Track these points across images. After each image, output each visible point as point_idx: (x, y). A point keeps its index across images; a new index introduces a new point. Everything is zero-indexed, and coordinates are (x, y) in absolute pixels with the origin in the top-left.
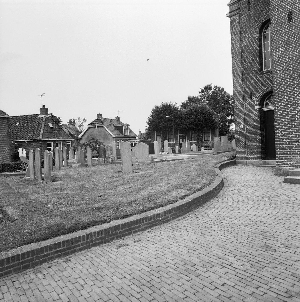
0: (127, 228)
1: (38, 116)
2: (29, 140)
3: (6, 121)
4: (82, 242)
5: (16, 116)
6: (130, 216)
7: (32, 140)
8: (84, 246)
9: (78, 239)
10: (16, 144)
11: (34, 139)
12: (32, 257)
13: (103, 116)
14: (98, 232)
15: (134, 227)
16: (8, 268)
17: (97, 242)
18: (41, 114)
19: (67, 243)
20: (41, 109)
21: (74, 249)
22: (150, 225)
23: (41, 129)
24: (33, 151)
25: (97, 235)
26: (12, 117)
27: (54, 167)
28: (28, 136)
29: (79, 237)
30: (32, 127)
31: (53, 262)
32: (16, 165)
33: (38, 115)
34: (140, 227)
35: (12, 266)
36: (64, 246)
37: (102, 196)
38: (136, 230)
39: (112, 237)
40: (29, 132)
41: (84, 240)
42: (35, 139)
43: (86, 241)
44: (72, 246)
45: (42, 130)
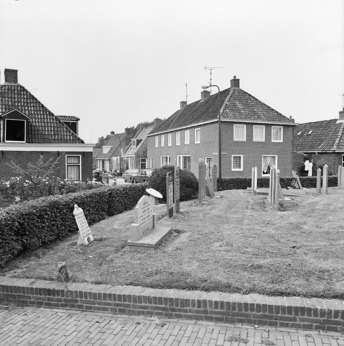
0: (267, 313)
1: (336, 122)
2: (320, 152)
3: (291, 129)
4: (190, 308)
5: (311, 123)
6: (286, 296)
7: (324, 151)
8: (193, 314)
9: (186, 302)
10: (305, 155)
11: (326, 151)
12: (128, 303)
13: (295, 122)
14: (216, 303)
15: (282, 317)
16: (105, 304)
17: (214, 316)
18: (341, 118)
19: (170, 301)
20: (340, 113)
21: (179, 313)
22: (318, 324)
23: (336, 138)
24: (328, 166)
25: (213, 306)
26: (297, 125)
27: (321, 188)
28: (320, 147)
29: (187, 301)
30: (326, 136)
31: (150, 318)
32: (290, 181)
33: (336, 120)
34: (296, 321)
35: (109, 304)
36: (166, 304)
37: (295, 248)
38: (286, 322)
39: (240, 318)
40: (322, 142)
41: (194, 306)
42: (328, 150)
43: (196, 308)
44: (177, 308)
45: (337, 139)
